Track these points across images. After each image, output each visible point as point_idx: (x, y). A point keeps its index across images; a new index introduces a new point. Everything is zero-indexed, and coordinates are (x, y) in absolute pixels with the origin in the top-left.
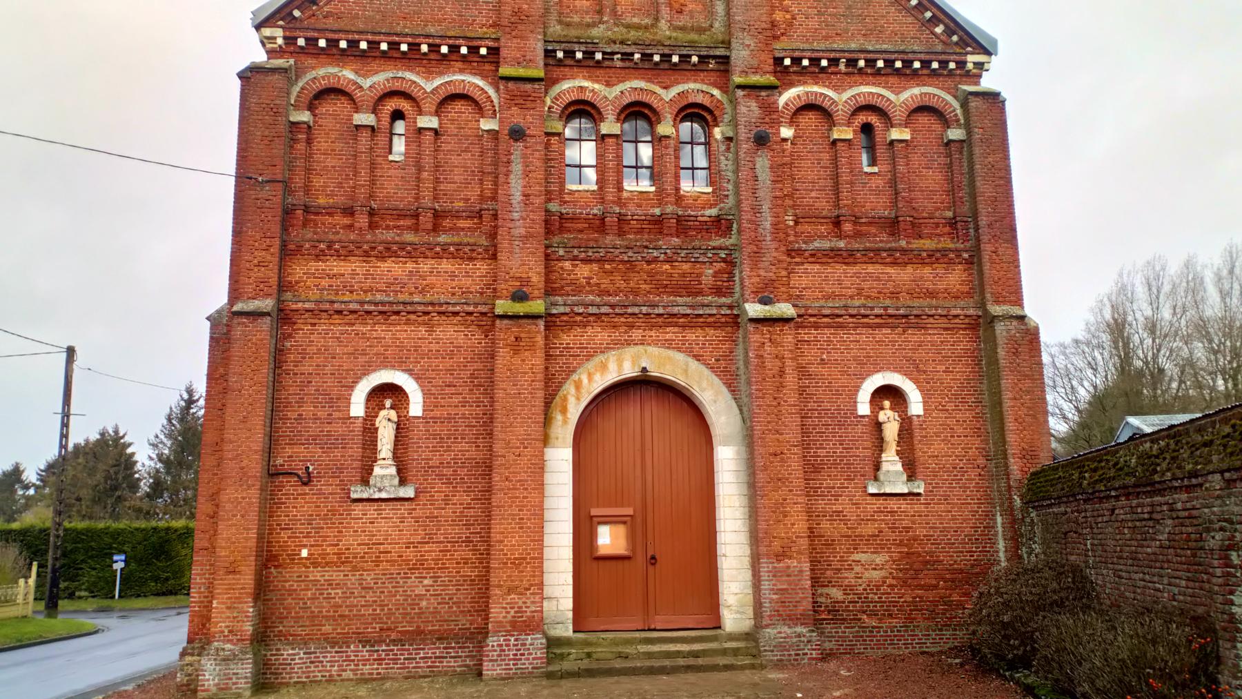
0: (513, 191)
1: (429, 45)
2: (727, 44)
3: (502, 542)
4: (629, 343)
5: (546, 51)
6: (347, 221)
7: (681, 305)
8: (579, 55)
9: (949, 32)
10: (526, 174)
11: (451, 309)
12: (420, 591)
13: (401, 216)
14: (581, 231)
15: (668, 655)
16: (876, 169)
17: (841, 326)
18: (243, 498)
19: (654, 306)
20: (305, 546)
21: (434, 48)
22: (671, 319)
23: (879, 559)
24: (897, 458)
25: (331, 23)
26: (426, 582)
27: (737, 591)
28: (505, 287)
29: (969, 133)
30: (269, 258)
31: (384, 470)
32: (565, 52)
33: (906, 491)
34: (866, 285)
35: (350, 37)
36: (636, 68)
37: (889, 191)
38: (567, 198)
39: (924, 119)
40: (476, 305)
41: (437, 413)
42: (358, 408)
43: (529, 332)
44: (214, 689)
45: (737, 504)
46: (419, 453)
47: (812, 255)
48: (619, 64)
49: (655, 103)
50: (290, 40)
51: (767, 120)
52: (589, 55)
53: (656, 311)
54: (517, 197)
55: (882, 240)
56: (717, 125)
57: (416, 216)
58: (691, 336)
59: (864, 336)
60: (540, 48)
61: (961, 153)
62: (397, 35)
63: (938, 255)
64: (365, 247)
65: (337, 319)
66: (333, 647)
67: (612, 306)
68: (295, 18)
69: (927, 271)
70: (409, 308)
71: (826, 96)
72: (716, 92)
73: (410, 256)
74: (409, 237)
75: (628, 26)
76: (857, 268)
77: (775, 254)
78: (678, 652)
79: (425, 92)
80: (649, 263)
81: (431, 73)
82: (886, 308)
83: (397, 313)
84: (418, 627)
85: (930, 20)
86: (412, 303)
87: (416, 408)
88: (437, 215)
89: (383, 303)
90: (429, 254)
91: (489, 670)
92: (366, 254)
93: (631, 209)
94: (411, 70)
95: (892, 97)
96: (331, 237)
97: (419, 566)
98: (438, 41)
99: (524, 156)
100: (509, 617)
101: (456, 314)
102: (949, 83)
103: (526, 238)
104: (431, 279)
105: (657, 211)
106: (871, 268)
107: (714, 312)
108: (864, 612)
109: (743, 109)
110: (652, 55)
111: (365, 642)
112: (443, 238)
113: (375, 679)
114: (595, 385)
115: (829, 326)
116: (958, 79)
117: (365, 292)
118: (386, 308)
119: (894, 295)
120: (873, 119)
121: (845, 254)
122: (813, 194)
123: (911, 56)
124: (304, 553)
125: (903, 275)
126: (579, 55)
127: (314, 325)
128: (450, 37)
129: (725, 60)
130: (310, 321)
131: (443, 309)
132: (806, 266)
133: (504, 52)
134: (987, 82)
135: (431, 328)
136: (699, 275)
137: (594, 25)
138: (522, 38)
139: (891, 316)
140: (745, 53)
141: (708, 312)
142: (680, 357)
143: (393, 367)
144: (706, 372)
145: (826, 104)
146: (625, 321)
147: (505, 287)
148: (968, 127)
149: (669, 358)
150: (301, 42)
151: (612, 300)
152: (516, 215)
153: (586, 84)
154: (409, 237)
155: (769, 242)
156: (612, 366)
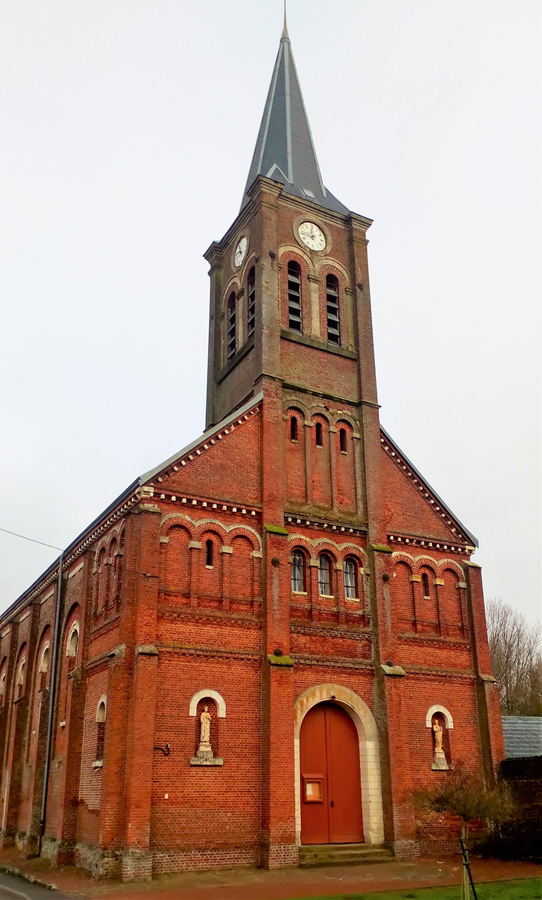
0: (274, 594)
1: (227, 507)
2: (367, 525)
3: (275, 792)
4: (324, 681)
5: (285, 517)
6: (184, 601)
7: (348, 662)
8: (299, 521)
9: (458, 532)
11: (240, 656)
12: (226, 820)
13: (211, 601)
14: (299, 617)
15: (353, 856)
16: (429, 598)
17: (418, 679)
18: (144, 763)
19: (336, 662)
20: (166, 792)
21: (230, 508)
22: (344, 670)
24: (442, 751)
26: (228, 815)
27: (377, 822)
28: (271, 647)
29: (469, 585)
31: (205, 748)
32: (293, 519)
34: (428, 658)
35: (188, 497)
36: (324, 531)
37: (435, 610)
38: (293, 598)
40: (253, 655)
41: (233, 716)
42: (193, 712)
43: (286, 674)
44: (132, 876)
45: (376, 774)
46: (224, 739)
47: (405, 641)
48: (316, 528)
49: (335, 552)
50: (157, 494)
51: (388, 569)
52: (303, 522)
53: (337, 665)
54: (276, 598)
55: (432, 635)
56: (361, 566)
57: (220, 601)
58: (353, 679)
59: (427, 684)
60: (282, 515)
61: (464, 594)
62: (212, 499)
63: (457, 646)
64: (197, 617)
65: (182, 658)
66: (183, 852)
67: (318, 661)
68: (158, 481)
69: (453, 653)
71: (409, 558)
72: (361, 549)
73: (219, 624)
74: (218, 614)
75: (319, 508)
76: (423, 649)
77: (393, 640)
78: (356, 854)
79: (226, 532)
80: (333, 638)
81: (226, 521)
82: (437, 671)
83: (213, 657)
84: (225, 841)
85: (450, 525)
86: (221, 652)
87: (222, 713)
88: (232, 602)
89: (206, 651)
90: (228, 624)
91: (272, 864)
92: (197, 622)
93: (323, 607)
94: (216, 518)
95: (436, 562)
96: (179, 610)
97: (224, 805)
98: (232, 505)
99: (279, 576)
100: (280, 834)
101: (242, 659)
102: (458, 557)
103: (281, 620)
105: (335, 609)
106: (430, 650)
107: (364, 667)
108: (431, 833)
109: (377, 562)
110: (332, 526)
111: (199, 850)
112: (234, 616)
113: (204, 871)
114: (310, 704)
115: (413, 679)
116: (461, 556)
117: (196, 643)
118: (208, 654)
119: (439, 664)
121: (419, 641)
122: (403, 608)
123: (443, 543)
124: (167, 796)
125: (443, 654)
126: (299, 521)
128: (238, 504)
129: (365, 533)
130: (168, 658)
132: (403, 646)
133: (265, 516)
134: (474, 560)
135: (229, 666)
136: (356, 646)
137: (302, 505)
139: (439, 676)
140: (375, 531)
141: (361, 667)
142: (348, 691)
143: (210, 688)
144: (361, 700)
145: (409, 562)
146: (324, 669)
147: (271, 647)
148: (468, 581)
149: (344, 691)
150: (163, 496)
152: (276, 608)
153: (303, 537)
154: (218, 614)
155: (390, 634)
156: (318, 694)
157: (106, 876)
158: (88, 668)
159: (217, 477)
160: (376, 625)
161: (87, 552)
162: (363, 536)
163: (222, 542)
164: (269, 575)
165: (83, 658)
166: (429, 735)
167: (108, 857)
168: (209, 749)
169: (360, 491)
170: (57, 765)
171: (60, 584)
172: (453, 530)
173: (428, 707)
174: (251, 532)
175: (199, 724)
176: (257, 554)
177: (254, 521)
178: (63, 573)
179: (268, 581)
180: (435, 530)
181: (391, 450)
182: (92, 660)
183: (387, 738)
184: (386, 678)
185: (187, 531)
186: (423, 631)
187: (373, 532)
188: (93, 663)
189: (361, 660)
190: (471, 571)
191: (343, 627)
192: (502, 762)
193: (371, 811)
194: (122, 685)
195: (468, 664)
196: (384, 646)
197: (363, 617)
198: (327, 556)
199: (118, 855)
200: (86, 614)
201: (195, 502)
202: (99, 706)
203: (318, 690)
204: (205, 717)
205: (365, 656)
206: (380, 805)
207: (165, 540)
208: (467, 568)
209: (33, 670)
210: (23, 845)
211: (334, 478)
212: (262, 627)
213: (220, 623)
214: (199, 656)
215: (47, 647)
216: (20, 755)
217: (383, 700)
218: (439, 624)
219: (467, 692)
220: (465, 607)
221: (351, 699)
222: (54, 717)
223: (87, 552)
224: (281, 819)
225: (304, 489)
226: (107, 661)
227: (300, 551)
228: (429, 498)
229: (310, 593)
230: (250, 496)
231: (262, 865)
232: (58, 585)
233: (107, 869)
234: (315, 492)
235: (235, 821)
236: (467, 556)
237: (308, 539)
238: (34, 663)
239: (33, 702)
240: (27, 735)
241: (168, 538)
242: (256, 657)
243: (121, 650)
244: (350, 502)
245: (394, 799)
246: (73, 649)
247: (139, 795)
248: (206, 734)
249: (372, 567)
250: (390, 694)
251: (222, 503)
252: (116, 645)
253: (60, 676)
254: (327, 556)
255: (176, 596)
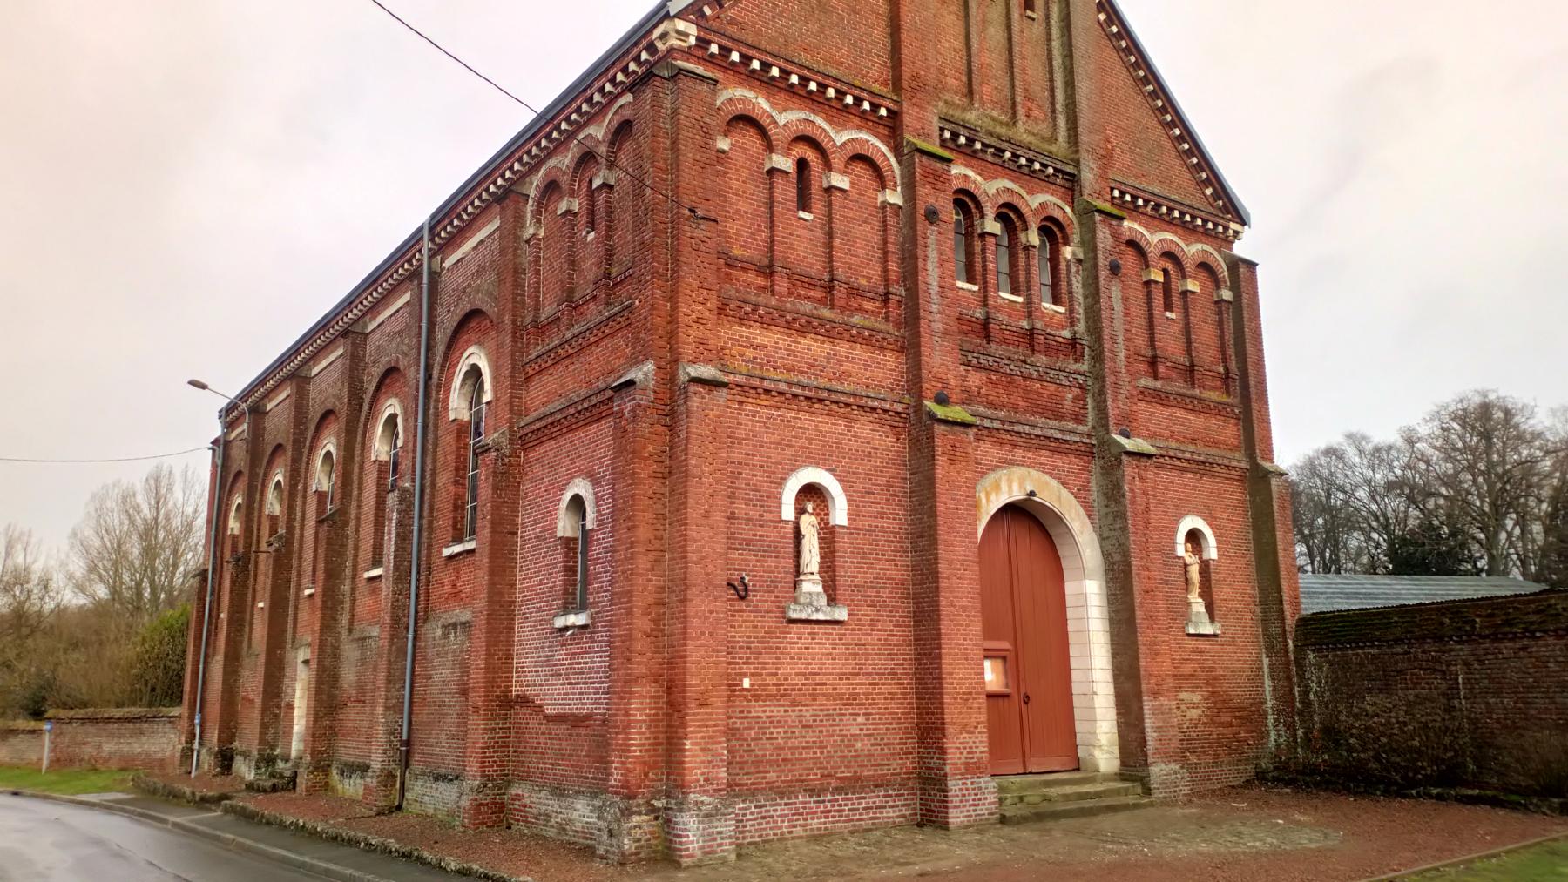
2: (1077, 163)
4: (1013, 463)
6: (761, 281)
7: (1052, 427)
9: (1216, 196)
10: (941, 263)
11: (870, 403)
12: (854, 730)
20: (745, 675)
23: (1196, 698)
25: (732, 30)
26: (860, 719)
28: (929, 388)
30: (707, 314)
31: (812, 586)
33: (1211, 632)
34: (1177, 428)
39: (859, 168)
41: (859, 524)
42: (788, 512)
44: (698, 853)
46: (846, 569)
48: (990, 158)
49: (1024, 210)
50: (703, 43)
54: (934, 289)
55: (1179, 386)
56: (1067, 243)
57: (830, 289)
59: (1176, 478)
60: (936, 124)
64: (789, 317)
67: (1003, 422)
69: (1213, 421)
70: (833, 397)
72: (1068, 210)
76: (1168, 412)
83: (821, 401)
89: (810, 388)
90: (846, 336)
91: (956, 817)
92: (789, 325)
97: (851, 701)
98: (845, 88)
99: (938, 242)
101: (874, 409)
103: (945, 333)
104: (847, 366)
105: (1025, 324)
106: (1179, 413)
111: (811, 791)
112: (856, 319)
118: (812, 394)
120: (811, 156)
124: (746, 683)
127: (741, 403)
131: (863, 402)
133: (907, 120)
134: (1240, 249)
136: (1063, 398)
137: (964, 109)
138: (921, 107)
142: (1054, 483)
144: (1074, 501)
145: (1143, 243)
146: (1017, 441)
148: (1235, 287)
151: (1002, 414)
152: (934, 308)
154: (826, 313)
156: (1004, 487)
157: (637, 853)
158: (526, 430)
159: (814, 27)
160: (1098, 358)
161: (508, 196)
162: (1068, 185)
163: (828, 166)
164: (921, 241)
165: (511, 411)
166: (1179, 570)
167: (640, 814)
168: (819, 588)
169: (1060, 96)
170: (439, 632)
171: (425, 280)
172: (1209, 191)
173: (1178, 518)
174: (879, 150)
175: (798, 536)
176: (894, 197)
177: (882, 130)
178: (430, 258)
179: (920, 253)
180: (1181, 188)
181: (1110, 21)
182: (533, 415)
183: (1127, 573)
184: (1125, 458)
185: (762, 131)
186: (1167, 379)
187: (1088, 176)
188: (540, 419)
189: (1071, 425)
190: (1242, 270)
191: (1041, 359)
192: (1300, 620)
193: (1098, 711)
194: (651, 448)
195: (1236, 442)
196: (1115, 399)
197: (1073, 342)
198: (1010, 216)
199: (659, 809)
200: (514, 322)
201: (775, 72)
202: (564, 503)
203: (1004, 479)
204: (809, 524)
205: (1079, 419)
206: (1112, 699)
207: (723, 144)
208: (1235, 264)
209: (357, 459)
210: (366, 787)
211: (1017, 61)
212: (910, 348)
213: (831, 332)
214: (795, 396)
215: (240, 500)
216: (335, 619)
217: (1118, 502)
218: (1192, 365)
219: (1234, 494)
220: (1230, 338)
221: (1059, 498)
222: (424, 540)
223: (508, 196)
224: (964, 728)
225: (964, 78)
226: (610, 399)
227: (966, 202)
228: (1172, 125)
229: (985, 288)
230: (874, 72)
231: (931, 817)
232: (421, 283)
233: (639, 840)
234: (985, 88)
235: (872, 731)
236: (1229, 242)
237: (979, 178)
238: (358, 446)
239: (358, 519)
240: (348, 581)
241: (728, 141)
242: (899, 407)
243: (645, 372)
244: (1042, 116)
245: (1144, 687)
246: (465, 405)
247: (703, 680)
248: (812, 556)
249: (1090, 245)
250: (1132, 491)
251: (827, 82)
252: (635, 361)
253: (435, 461)
254: (1010, 216)
255: (744, 269)
